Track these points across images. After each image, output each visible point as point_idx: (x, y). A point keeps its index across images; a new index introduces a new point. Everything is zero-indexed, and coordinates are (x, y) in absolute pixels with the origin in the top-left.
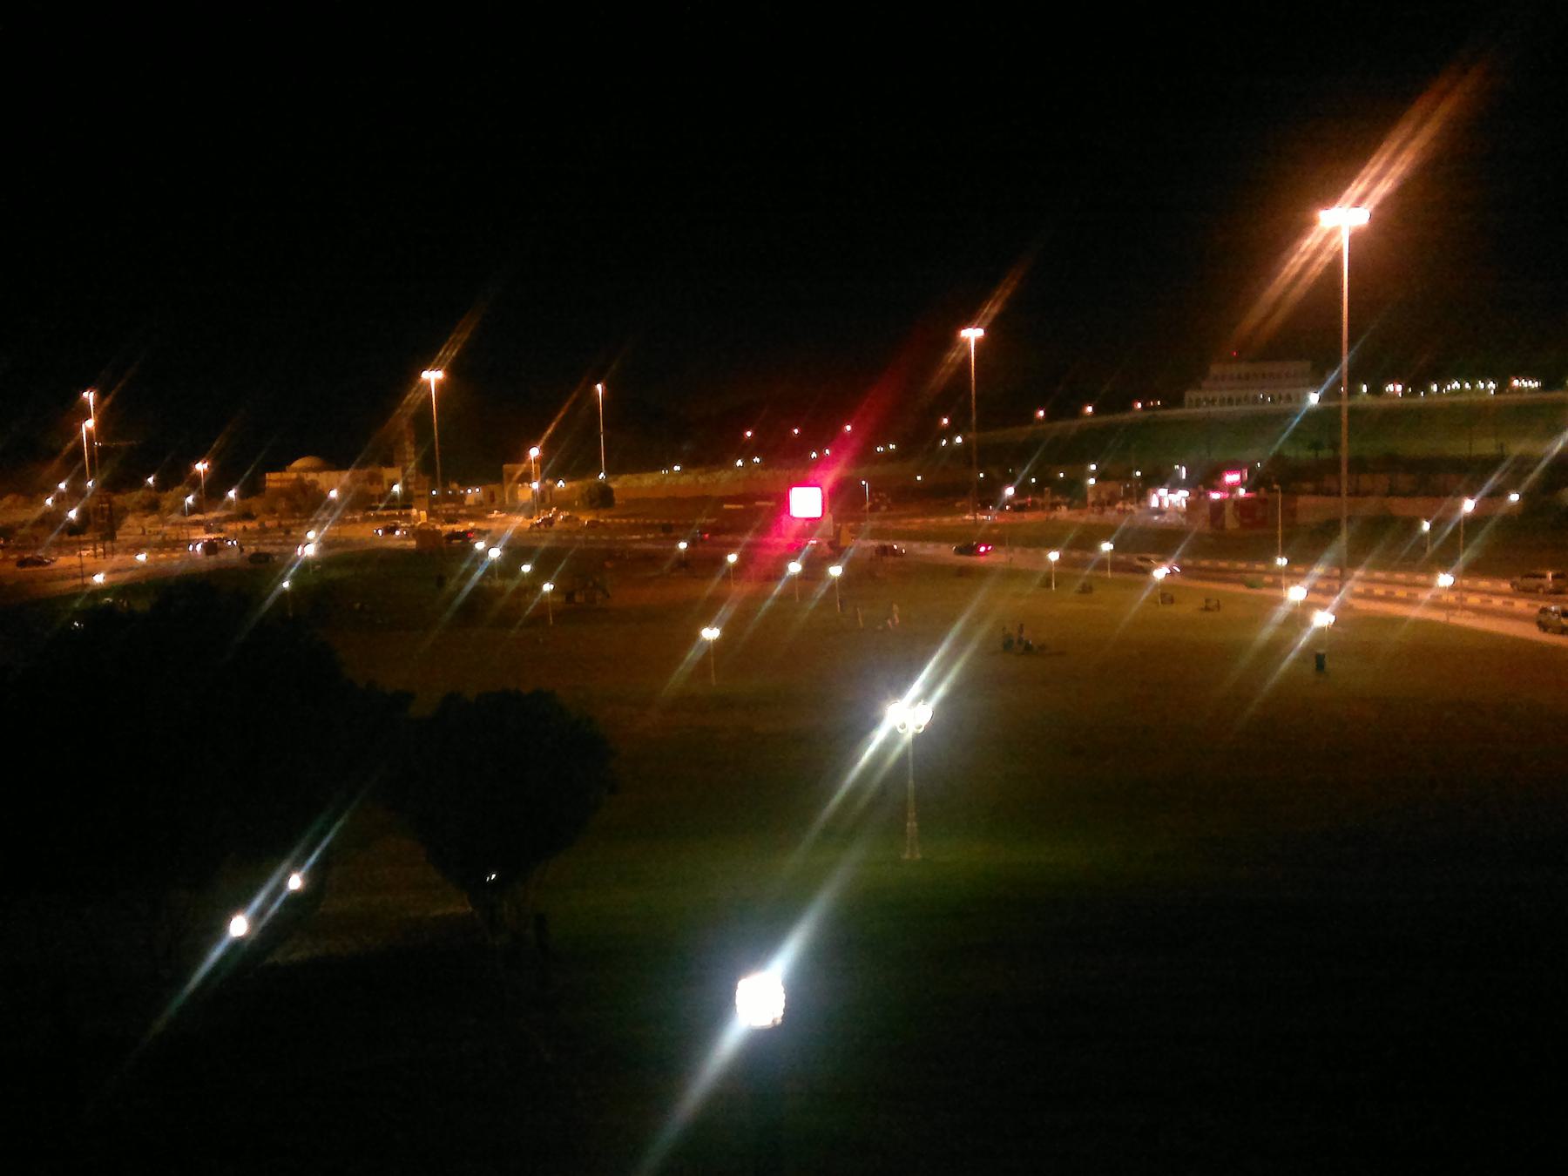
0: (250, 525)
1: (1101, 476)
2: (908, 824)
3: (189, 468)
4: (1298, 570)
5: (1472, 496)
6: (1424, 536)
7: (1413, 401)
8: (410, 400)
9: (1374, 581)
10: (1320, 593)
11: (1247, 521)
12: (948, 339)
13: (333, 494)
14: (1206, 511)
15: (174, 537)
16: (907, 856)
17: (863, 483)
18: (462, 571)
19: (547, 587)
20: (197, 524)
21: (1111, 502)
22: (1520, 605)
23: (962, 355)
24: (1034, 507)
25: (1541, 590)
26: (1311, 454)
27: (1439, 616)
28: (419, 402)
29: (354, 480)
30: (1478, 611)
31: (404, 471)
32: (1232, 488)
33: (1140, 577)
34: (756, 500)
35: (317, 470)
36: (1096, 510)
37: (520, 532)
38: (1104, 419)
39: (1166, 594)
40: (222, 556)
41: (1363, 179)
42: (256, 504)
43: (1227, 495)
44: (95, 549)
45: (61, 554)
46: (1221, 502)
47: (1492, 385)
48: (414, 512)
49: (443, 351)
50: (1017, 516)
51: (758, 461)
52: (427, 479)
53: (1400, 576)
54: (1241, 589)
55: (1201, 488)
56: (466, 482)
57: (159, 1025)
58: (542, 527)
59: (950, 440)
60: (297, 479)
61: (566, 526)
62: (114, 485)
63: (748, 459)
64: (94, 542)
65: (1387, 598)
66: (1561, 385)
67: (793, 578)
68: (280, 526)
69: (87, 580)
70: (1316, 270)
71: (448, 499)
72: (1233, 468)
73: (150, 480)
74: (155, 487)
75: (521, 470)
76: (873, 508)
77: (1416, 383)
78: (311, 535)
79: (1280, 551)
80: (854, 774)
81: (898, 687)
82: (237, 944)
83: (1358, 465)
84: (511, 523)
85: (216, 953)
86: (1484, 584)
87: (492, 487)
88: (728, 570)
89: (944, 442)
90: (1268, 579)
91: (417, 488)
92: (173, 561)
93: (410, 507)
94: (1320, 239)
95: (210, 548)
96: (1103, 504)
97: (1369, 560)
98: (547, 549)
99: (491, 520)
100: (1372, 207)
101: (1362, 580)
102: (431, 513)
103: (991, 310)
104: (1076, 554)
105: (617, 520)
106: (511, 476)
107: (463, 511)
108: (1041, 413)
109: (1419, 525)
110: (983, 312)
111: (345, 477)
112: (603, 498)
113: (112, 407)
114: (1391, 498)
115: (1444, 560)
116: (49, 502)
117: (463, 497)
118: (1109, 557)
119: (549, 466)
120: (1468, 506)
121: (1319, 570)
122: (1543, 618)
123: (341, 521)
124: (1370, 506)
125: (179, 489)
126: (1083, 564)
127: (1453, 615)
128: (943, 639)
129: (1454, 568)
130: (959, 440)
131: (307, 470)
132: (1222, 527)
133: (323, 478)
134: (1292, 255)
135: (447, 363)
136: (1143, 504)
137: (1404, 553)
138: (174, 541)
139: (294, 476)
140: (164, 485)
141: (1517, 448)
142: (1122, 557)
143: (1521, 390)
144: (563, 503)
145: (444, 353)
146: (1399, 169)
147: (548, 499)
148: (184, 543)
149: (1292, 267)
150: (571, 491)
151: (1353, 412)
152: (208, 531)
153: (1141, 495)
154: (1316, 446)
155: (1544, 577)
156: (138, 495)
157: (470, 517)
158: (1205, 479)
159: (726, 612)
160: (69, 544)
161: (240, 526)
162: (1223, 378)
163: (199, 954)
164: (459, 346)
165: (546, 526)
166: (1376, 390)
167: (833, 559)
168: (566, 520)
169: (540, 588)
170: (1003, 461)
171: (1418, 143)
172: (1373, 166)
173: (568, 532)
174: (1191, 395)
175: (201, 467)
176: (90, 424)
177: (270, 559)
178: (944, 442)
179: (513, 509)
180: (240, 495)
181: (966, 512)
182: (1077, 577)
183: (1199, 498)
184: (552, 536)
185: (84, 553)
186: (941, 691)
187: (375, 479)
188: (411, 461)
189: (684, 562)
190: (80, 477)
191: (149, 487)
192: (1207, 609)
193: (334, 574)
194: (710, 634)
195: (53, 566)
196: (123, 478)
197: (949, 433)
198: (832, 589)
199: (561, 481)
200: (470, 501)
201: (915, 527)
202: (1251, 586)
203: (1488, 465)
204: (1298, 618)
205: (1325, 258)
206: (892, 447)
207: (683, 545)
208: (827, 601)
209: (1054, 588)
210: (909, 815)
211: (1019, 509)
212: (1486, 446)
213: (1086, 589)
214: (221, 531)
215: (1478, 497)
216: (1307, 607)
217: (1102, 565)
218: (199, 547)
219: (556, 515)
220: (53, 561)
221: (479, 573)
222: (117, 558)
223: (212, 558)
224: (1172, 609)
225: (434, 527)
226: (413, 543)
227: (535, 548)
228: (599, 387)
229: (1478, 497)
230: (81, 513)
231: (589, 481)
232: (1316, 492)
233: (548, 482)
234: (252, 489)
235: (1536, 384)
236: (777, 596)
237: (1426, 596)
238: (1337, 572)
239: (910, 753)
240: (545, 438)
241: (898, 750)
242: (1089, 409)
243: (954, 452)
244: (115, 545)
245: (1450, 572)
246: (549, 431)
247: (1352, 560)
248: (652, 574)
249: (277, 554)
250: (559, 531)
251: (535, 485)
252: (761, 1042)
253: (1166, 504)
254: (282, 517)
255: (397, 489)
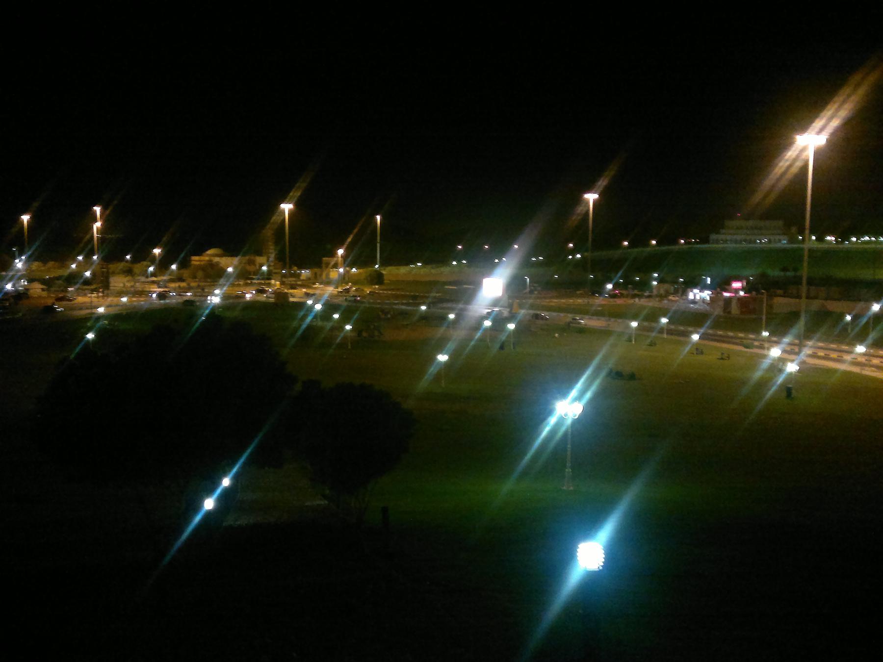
0: (183, 284)
1: (661, 281)
3: (150, 252)
4: (774, 339)
6: (848, 324)
7: (840, 246)
11: (744, 310)
12: (578, 200)
14: (721, 303)
15: (140, 289)
19: (348, 327)
20: (153, 282)
21: (668, 294)
23: (585, 209)
24: (621, 296)
26: (782, 274)
27: (856, 369)
31: (268, 260)
32: (737, 291)
33: (682, 339)
34: (464, 285)
37: (332, 296)
38: (664, 248)
39: (698, 349)
42: (186, 273)
45: (78, 295)
46: (730, 298)
50: (612, 300)
53: (833, 346)
55: (718, 290)
56: (301, 267)
57: (168, 558)
60: (208, 261)
62: (107, 259)
68: (199, 286)
69: (94, 311)
70: (794, 170)
72: (737, 279)
74: (131, 261)
75: (333, 261)
76: (531, 292)
77: (844, 236)
78: (217, 292)
79: (764, 326)
82: (209, 513)
84: (327, 290)
85: (198, 518)
87: (316, 270)
90: (756, 343)
91: (275, 269)
92: (141, 302)
95: (161, 296)
96: (661, 297)
97: (818, 335)
99: (315, 288)
102: (282, 283)
103: (602, 183)
104: (646, 324)
106: (327, 264)
107: (299, 283)
111: (236, 260)
112: (378, 278)
113: (109, 215)
115: (861, 338)
116: (74, 266)
117: (300, 275)
119: (349, 259)
121: (787, 340)
123: (233, 285)
125: (145, 263)
126: (651, 329)
129: (866, 342)
132: (729, 313)
133: (223, 261)
134: (780, 161)
136: (684, 297)
137: (836, 333)
138: (141, 291)
139: (207, 258)
140: (135, 260)
142: (672, 327)
147: (347, 279)
148: (146, 293)
150: (360, 273)
151: (811, 251)
152: (159, 287)
153: (684, 293)
154: (784, 269)
156: (121, 265)
158: (721, 284)
159: (451, 346)
166: (820, 239)
167: (509, 319)
170: (606, 270)
172: (829, 110)
175: (157, 251)
176: (98, 225)
179: (328, 283)
180: (179, 268)
182: (648, 336)
183: (717, 296)
186: (588, 395)
187: (251, 262)
189: (425, 317)
190: (88, 256)
191: (127, 261)
192: (722, 359)
194: (443, 358)
195: (75, 302)
196: (112, 255)
197: (573, 252)
198: (509, 336)
200: (303, 277)
202: (747, 347)
205: (799, 164)
207: (423, 308)
210: (568, 464)
213: (652, 344)
214: (166, 287)
216: (782, 361)
217: (661, 331)
218: (154, 295)
219: (351, 287)
220: (75, 299)
221: (309, 319)
222: (110, 299)
224: (700, 357)
226: (272, 300)
228: (378, 218)
232: (783, 296)
233: (347, 269)
234: (183, 265)
236: (478, 339)
237: (848, 358)
239: (570, 430)
243: (577, 263)
244: (109, 292)
245: (864, 344)
247: (808, 334)
248: (405, 323)
249: (198, 301)
251: (341, 270)
252: (592, 579)
255: (264, 268)
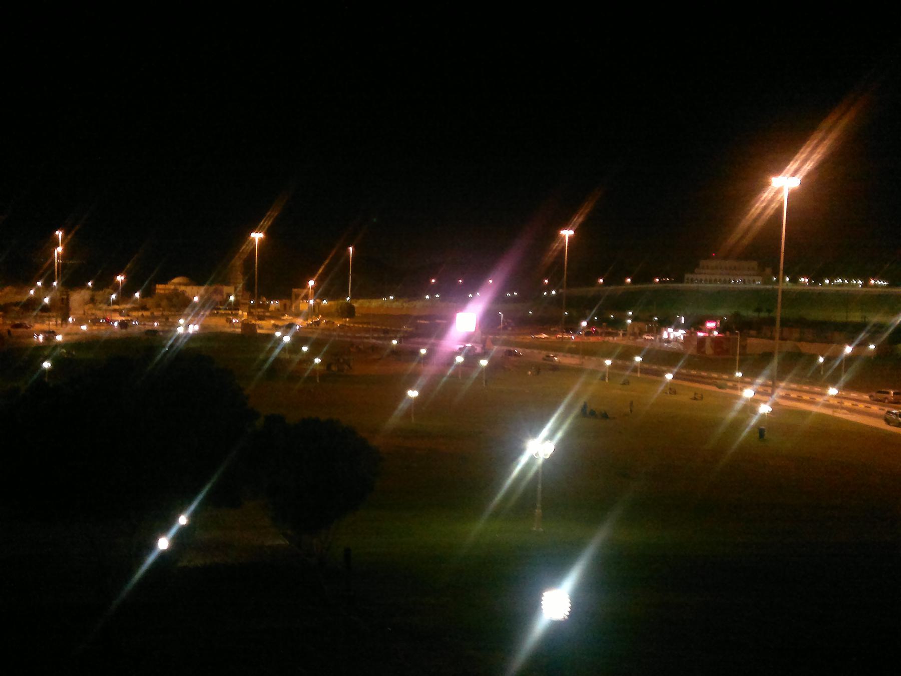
0: (146, 313)
1: (634, 319)
2: (537, 511)
5: (850, 345)
8: (243, 249)
9: (792, 390)
10: (764, 393)
12: (554, 236)
13: (196, 299)
16: (535, 529)
17: (500, 313)
18: (267, 349)
19: (317, 361)
20: (115, 311)
21: (641, 333)
22: (875, 408)
24: (596, 333)
25: (887, 401)
26: (756, 314)
27: (829, 412)
28: (249, 251)
29: (206, 291)
30: (850, 410)
32: (711, 330)
35: (186, 285)
36: (631, 339)
39: (672, 389)
40: (129, 330)
41: (797, 160)
42: (150, 302)
43: (708, 335)
44: (56, 322)
45: (36, 322)
46: (703, 338)
47: (860, 282)
48: (240, 312)
49: (263, 221)
51: (438, 296)
52: (248, 295)
53: (806, 388)
54: (713, 388)
55: (693, 329)
56: (270, 298)
58: (314, 326)
59: (549, 292)
61: (328, 326)
63: (432, 295)
64: (57, 317)
65: (799, 399)
66: (897, 286)
67: (458, 365)
68: (163, 315)
70: (770, 211)
71: (260, 306)
73: (90, 284)
74: (93, 288)
76: (505, 328)
77: (817, 278)
79: (737, 367)
80: (509, 482)
81: (535, 432)
83: (785, 323)
86: (853, 395)
87: (284, 301)
88: (421, 358)
89: (545, 293)
90: (730, 384)
92: (102, 331)
93: (238, 310)
94: (773, 194)
95: (123, 325)
97: (790, 376)
98: (317, 339)
100: (802, 177)
101: (784, 388)
102: (250, 314)
103: (578, 219)
104: (620, 362)
105: (356, 325)
107: (268, 314)
108: (601, 281)
109: (817, 358)
110: (573, 220)
111: (202, 290)
112: (349, 311)
114: (802, 343)
115: (833, 381)
116: (32, 292)
117: (268, 305)
118: (639, 366)
120: (848, 350)
121: (760, 381)
122: (888, 417)
124: (789, 346)
125: (108, 290)
126: (624, 368)
127: (835, 412)
128: (559, 406)
130: (554, 292)
131: (180, 284)
132: (704, 352)
133: (189, 290)
135: (266, 229)
139: (172, 287)
141: (875, 318)
142: (646, 366)
143: (876, 286)
144: (326, 313)
145: (264, 223)
146: (817, 157)
147: (317, 311)
149: (757, 209)
153: (659, 332)
154: (758, 310)
155: (888, 393)
157: (271, 317)
158: (695, 324)
160: (41, 317)
161: (140, 314)
162: (708, 268)
163: (140, 560)
164: (272, 219)
165: (315, 326)
166: (794, 280)
168: (326, 323)
169: (313, 361)
170: (581, 306)
171: (827, 143)
172: (802, 153)
173: (329, 329)
174: (688, 276)
175: (120, 278)
176: (59, 249)
177: (157, 334)
178: (545, 293)
179: (298, 315)
180: (142, 296)
181: (558, 333)
184: (319, 331)
185: (51, 323)
186: (559, 435)
188: (239, 283)
189: (396, 352)
192: (695, 399)
193: (192, 345)
194: (413, 394)
196: (73, 281)
197: (548, 288)
198: (481, 372)
199: (325, 300)
200: (272, 308)
201: (525, 341)
202: (720, 387)
203: (858, 327)
204: (750, 407)
205: (775, 205)
206: (515, 294)
207: (395, 342)
208: (479, 379)
209: (607, 381)
211: (588, 334)
212: (855, 317)
213: (626, 383)
214: (128, 316)
215: (854, 345)
217: (635, 370)
218: (116, 324)
219: (321, 320)
221: (277, 351)
223: (124, 331)
224: (674, 398)
225: (251, 322)
227: (310, 338)
228: (351, 249)
229: (854, 345)
230: (51, 300)
231: (341, 301)
233: (318, 300)
234: (148, 293)
235: (886, 283)
238: (770, 383)
240: (318, 275)
241: (534, 469)
242: (629, 280)
245: (836, 387)
246: (320, 271)
247: (781, 374)
250: (323, 329)
251: (312, 302)
253: (672, 337)
254: (164, 310)
255: (232, 298)
